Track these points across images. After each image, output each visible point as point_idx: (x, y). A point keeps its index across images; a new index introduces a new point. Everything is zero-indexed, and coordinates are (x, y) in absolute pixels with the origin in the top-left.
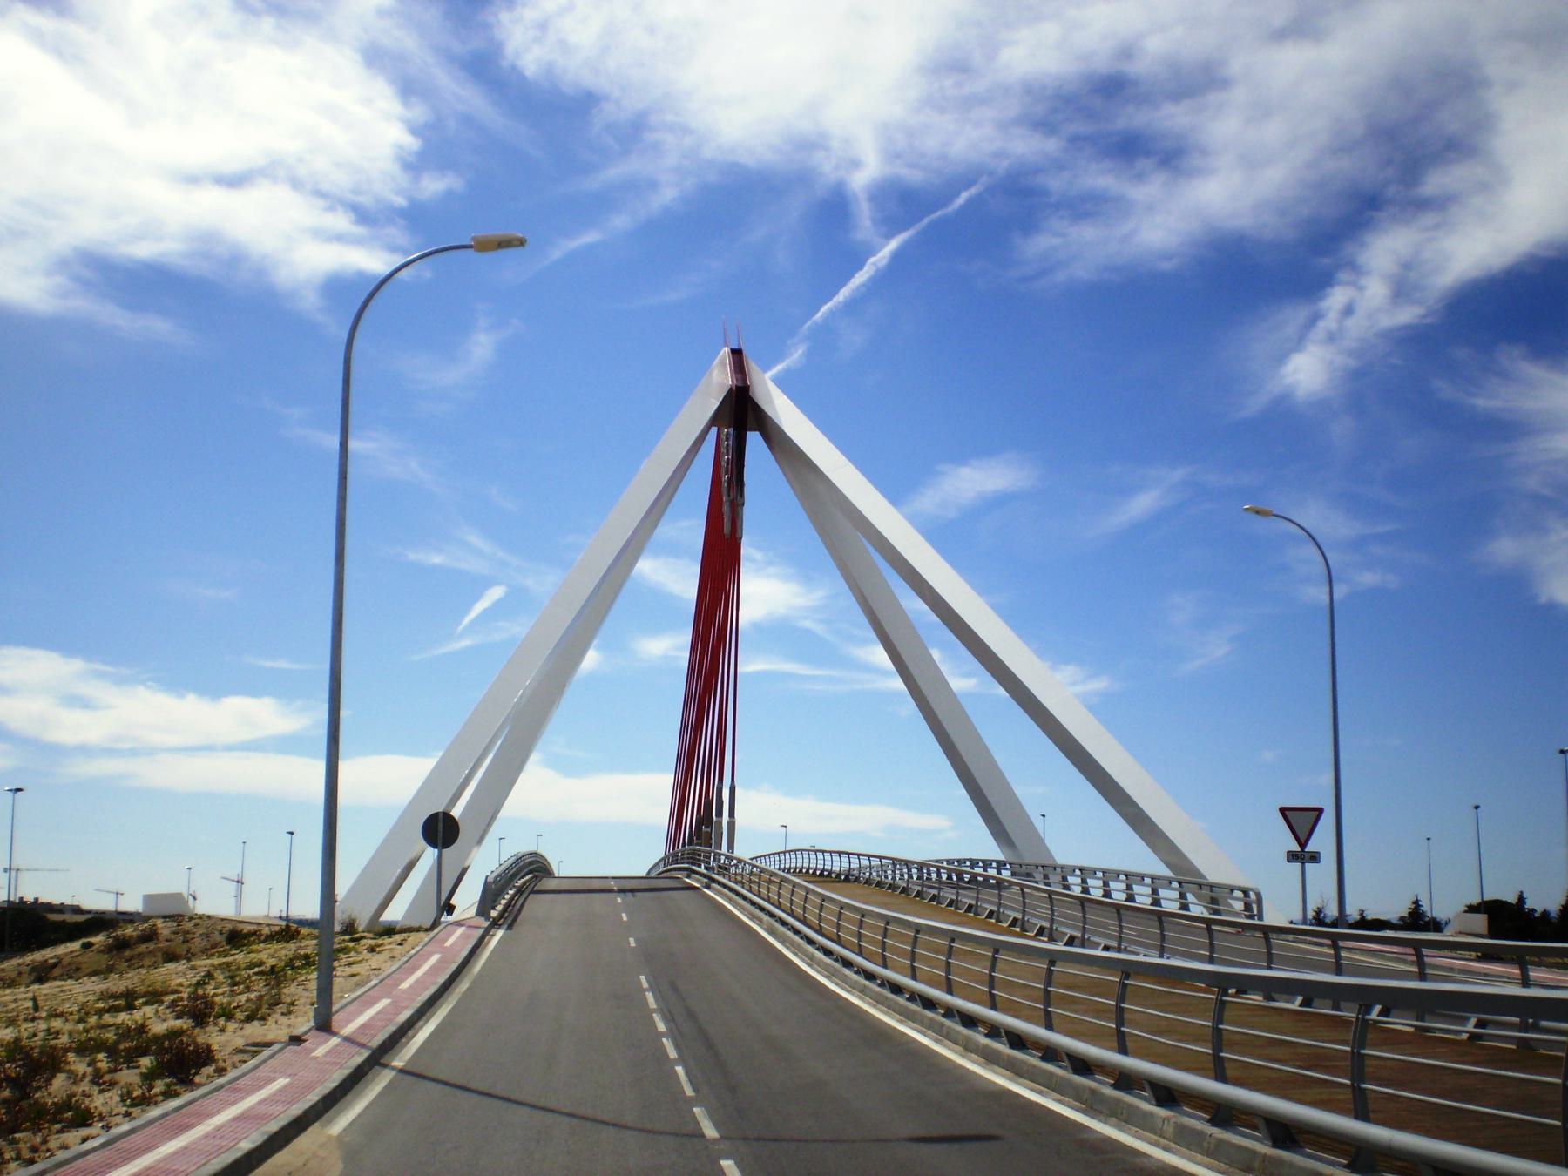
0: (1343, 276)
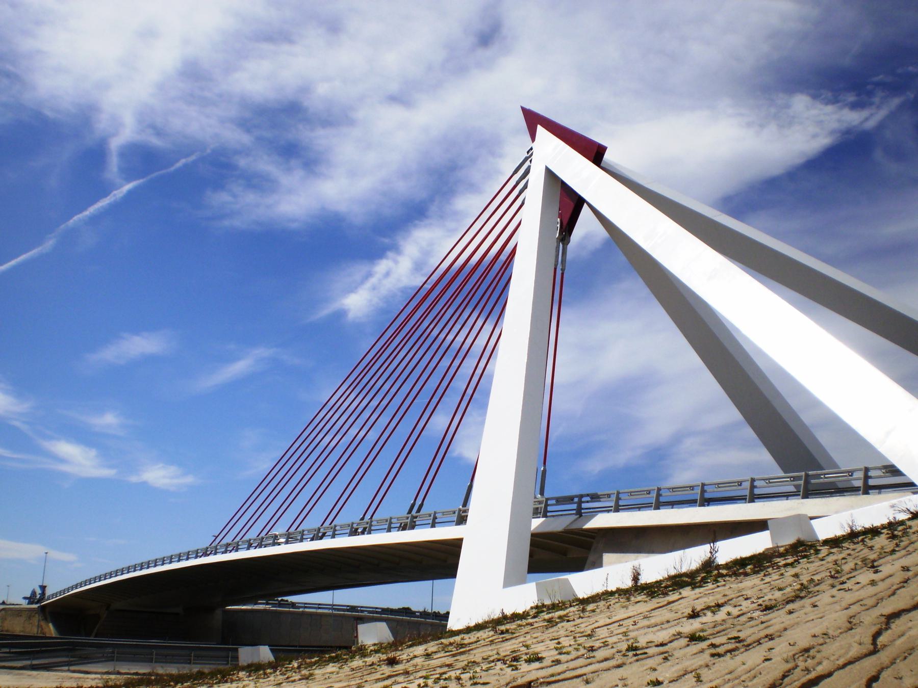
0: (390, 254)
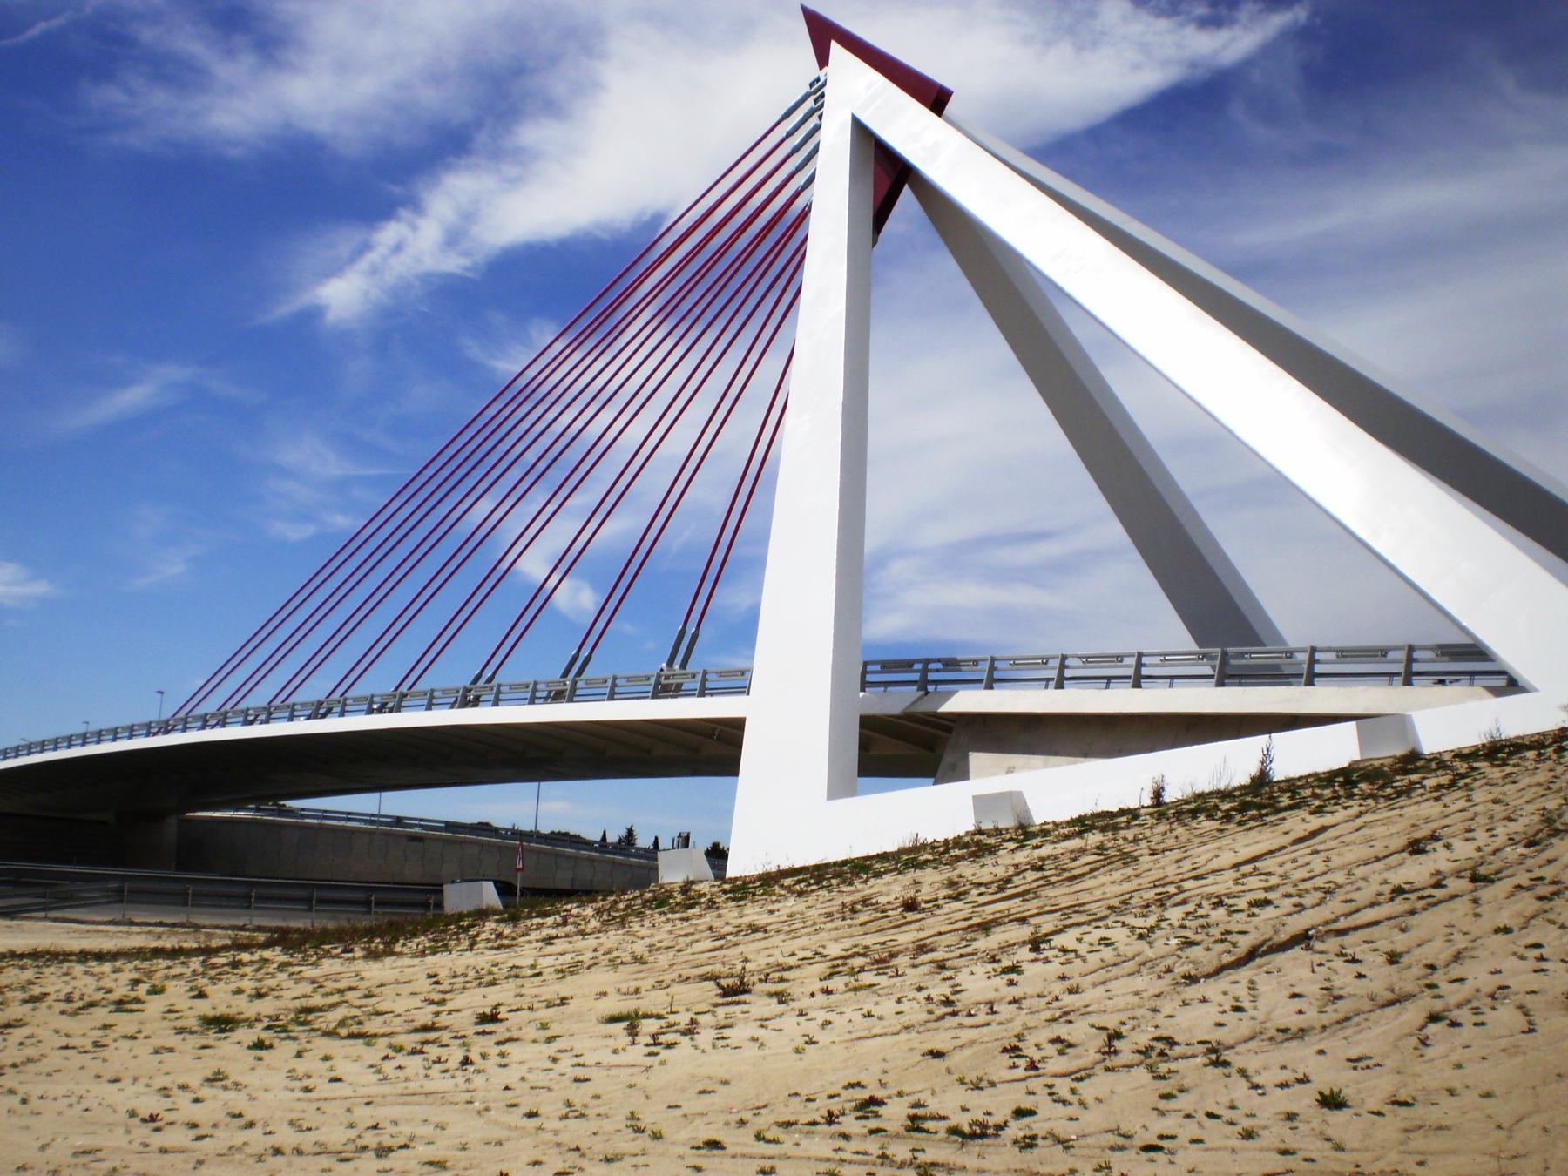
0: (404, 213)
